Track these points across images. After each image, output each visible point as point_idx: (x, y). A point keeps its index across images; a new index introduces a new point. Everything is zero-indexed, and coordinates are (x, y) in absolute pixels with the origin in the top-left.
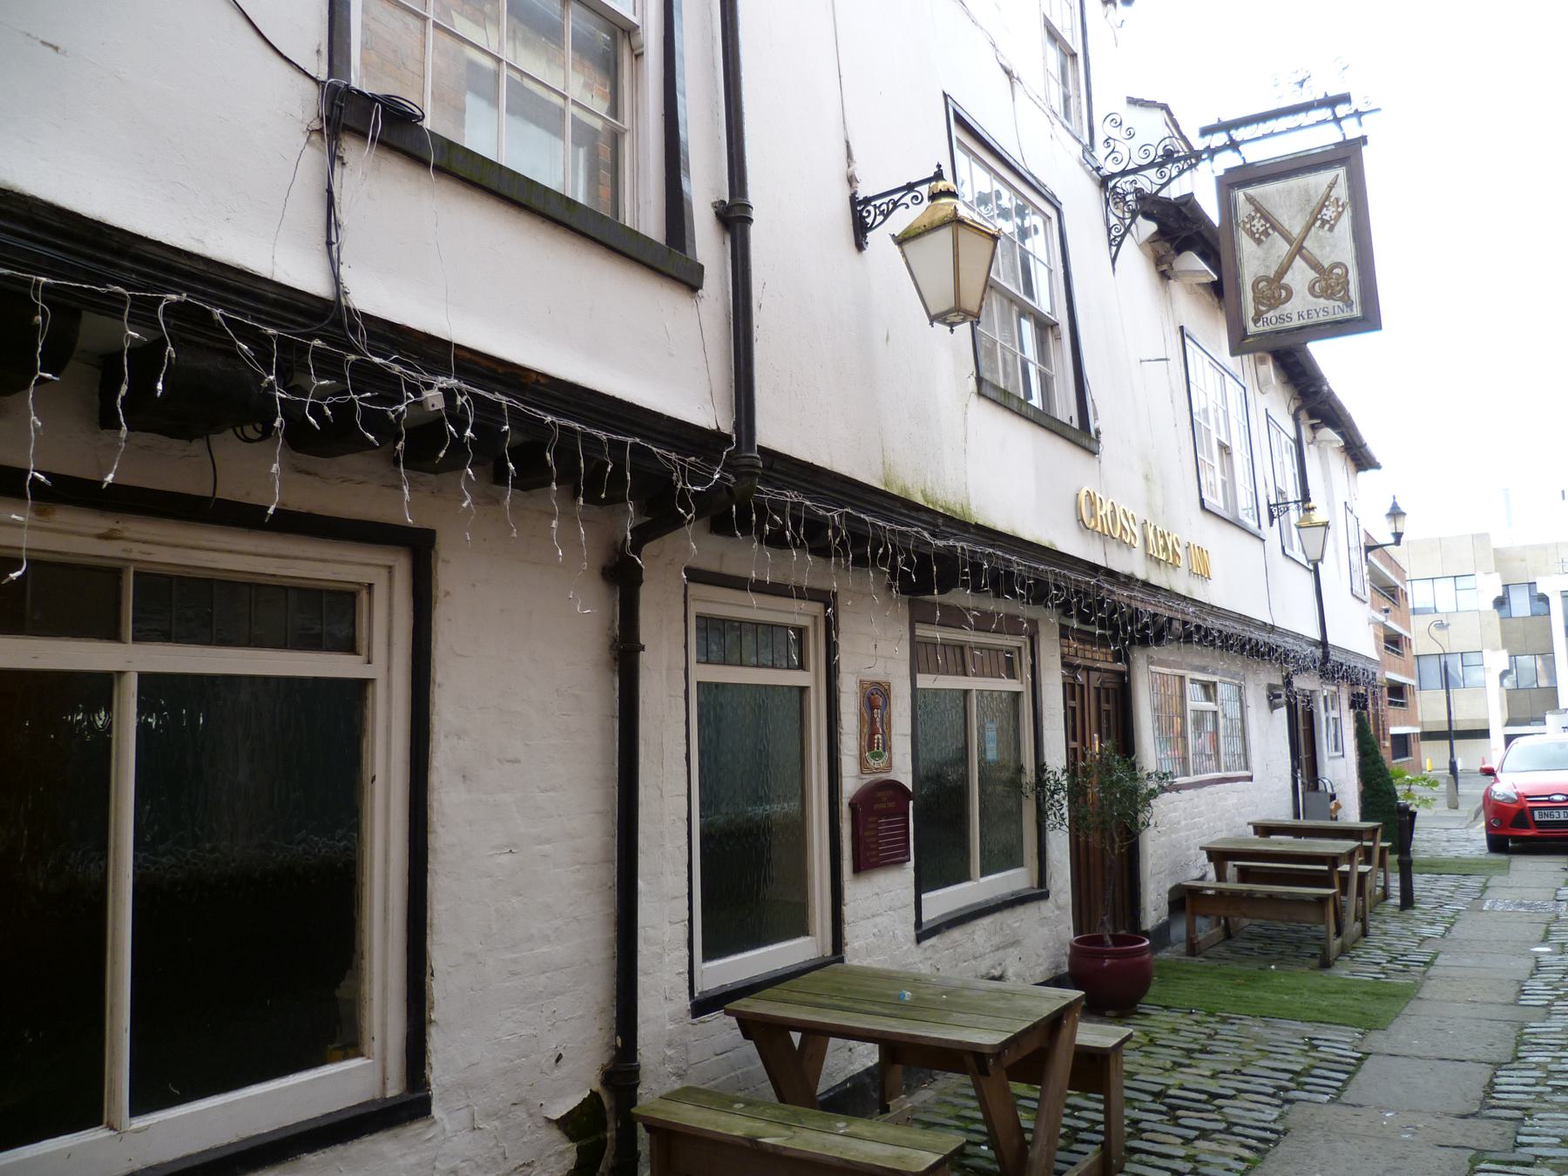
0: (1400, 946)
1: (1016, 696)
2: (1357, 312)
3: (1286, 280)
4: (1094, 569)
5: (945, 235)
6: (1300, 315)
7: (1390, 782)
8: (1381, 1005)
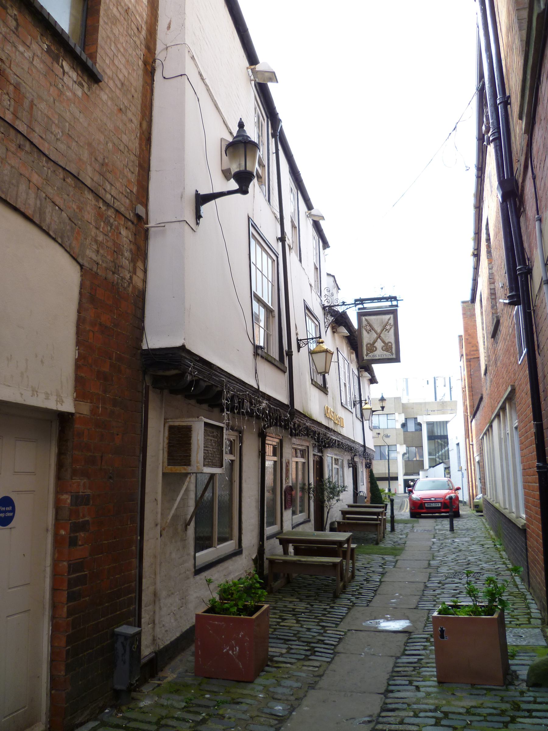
0: (395, 540)
2: (394, 356)
3: (375, 345)
4: (327, 428)
5: (324, 354)
6: (379, 356)
7: (380, 493)
8: (397, 550)
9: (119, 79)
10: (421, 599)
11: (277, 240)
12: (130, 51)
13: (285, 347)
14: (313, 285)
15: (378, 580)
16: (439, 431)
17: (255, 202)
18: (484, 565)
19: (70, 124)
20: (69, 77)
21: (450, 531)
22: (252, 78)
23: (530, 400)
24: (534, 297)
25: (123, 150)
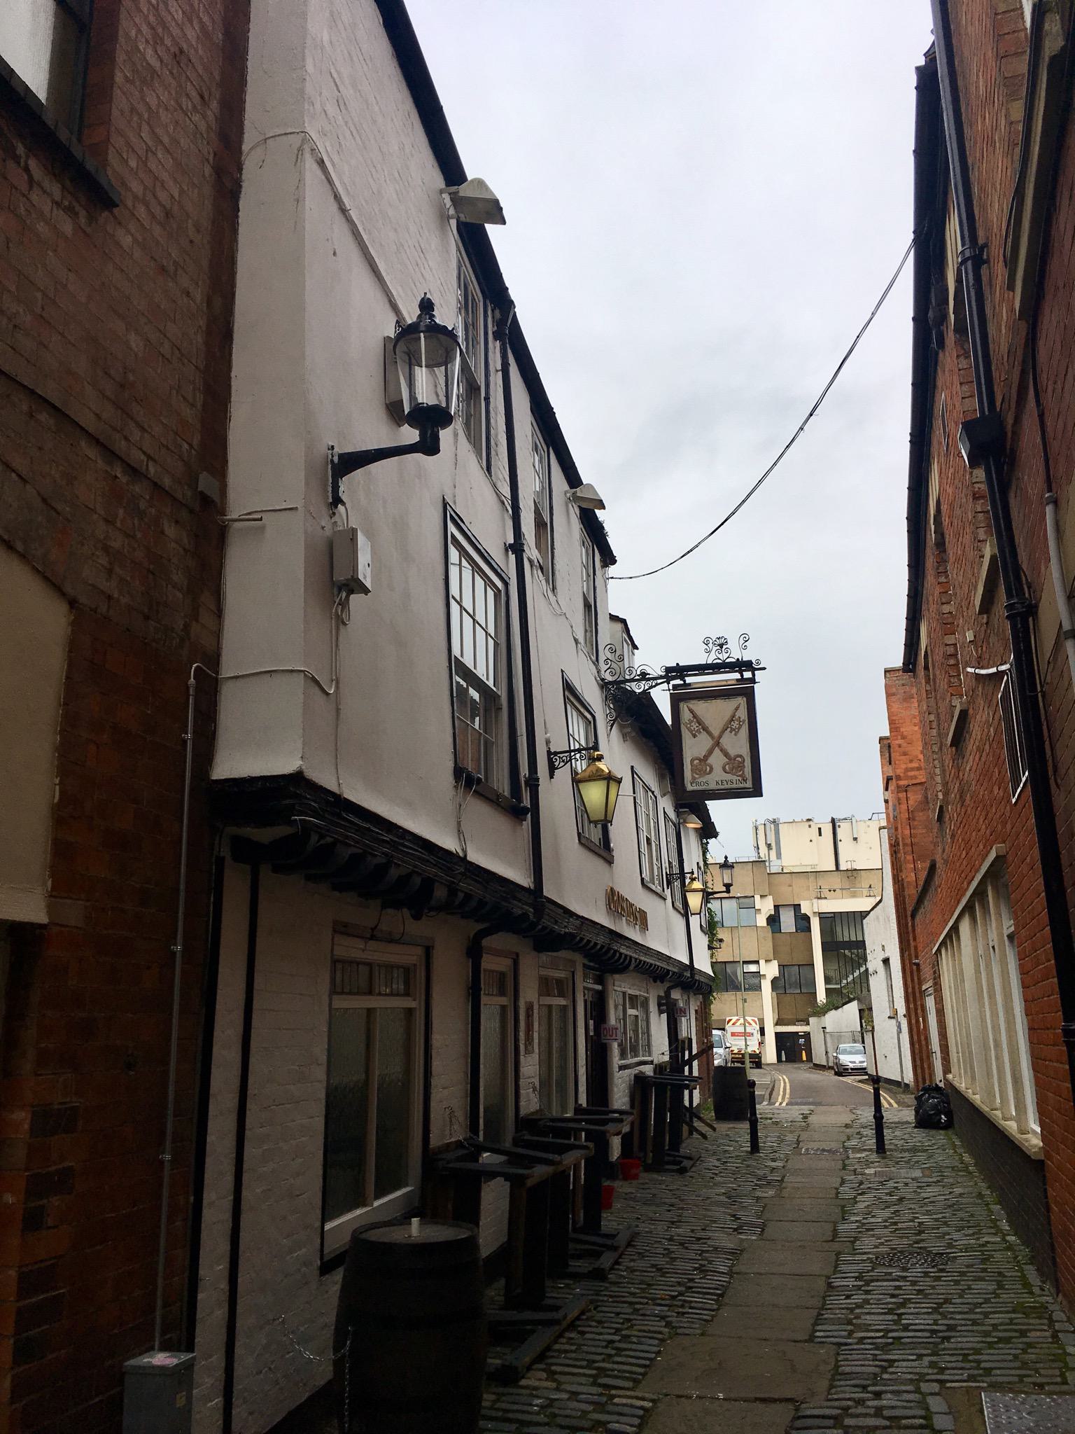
1: (410, 1012)
3: (710, 761)
9: (160, 203)
10: (818, 1320)
11: (506, 550)
12: (184, 142)
13: (524, 770)
14: (581, 640)
15: (723, 1269)
16: (846, 934)
17: (455, 467)
18: (956, 1236)
19: (44, 294)
20: (45, 192)
21: (877, 1152)
22: (452, 212)
23: (1041, 880)
24: (1044, 666)
25: (168, 356)
